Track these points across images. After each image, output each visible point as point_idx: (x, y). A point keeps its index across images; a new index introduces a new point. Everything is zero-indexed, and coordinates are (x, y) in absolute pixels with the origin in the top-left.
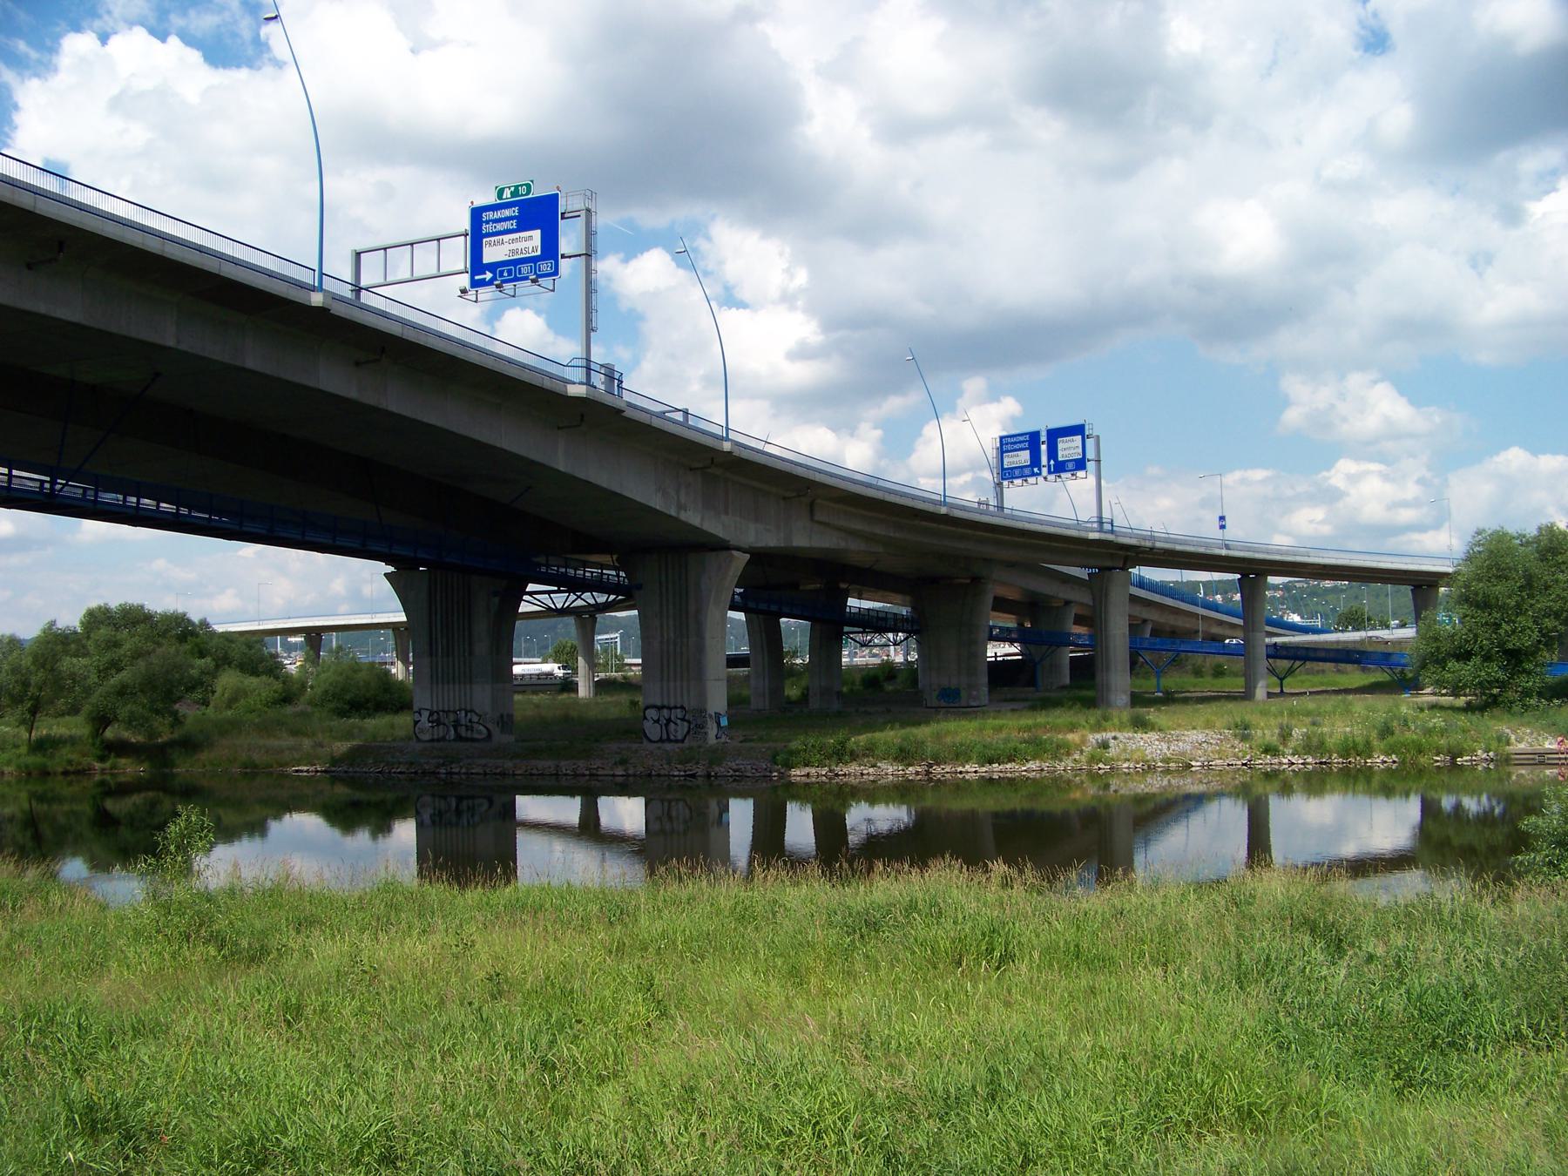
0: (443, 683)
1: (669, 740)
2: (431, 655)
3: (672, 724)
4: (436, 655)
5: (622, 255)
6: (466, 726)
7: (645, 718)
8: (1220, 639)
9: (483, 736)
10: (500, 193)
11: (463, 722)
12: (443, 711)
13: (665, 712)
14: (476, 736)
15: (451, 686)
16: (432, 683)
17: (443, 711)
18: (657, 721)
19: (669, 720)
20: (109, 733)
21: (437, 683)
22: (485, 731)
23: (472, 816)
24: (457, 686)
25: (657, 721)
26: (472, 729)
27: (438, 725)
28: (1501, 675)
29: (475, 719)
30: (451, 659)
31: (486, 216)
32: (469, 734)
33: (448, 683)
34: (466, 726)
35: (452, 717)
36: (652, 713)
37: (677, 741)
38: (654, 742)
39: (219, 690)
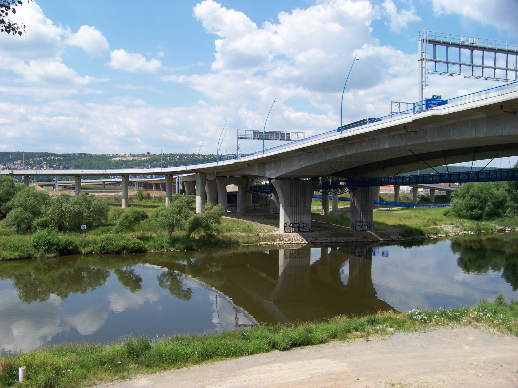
0: (302, 215)
1: (362, 231)
2: (291, 206)
3: (363, 226)
4: (293, 207)
5: (214, 53)
6: (302, 228)
7: (356, 225)
8: (88, 194)
9: (308, 231)
10: (433, 96)
11: (301, 226)
12: (295, 223)
13: (362, 223)
14: (305, 230)
15: (297, 216)
16: (291, 214)
17: (295, 223)
18: (359, 226)
19: (362, 225)
20: (174, 234)
21: (293, 215)
22: (308, 229)
23: (303, 255)
24: (299, 216)
25: (359, 226)
26: (304, 229)
27: (292, 228)
28: (411, 214)
29: (305, 225)
30: (297, 208)
31: (430, 102)
32: (303, 230)
33: (297, 215)
34: (302, 228)
35: (297, 225)
36: (358, 224)
37: (364, 231)
38: (356, 230)
39: (499, 210)
